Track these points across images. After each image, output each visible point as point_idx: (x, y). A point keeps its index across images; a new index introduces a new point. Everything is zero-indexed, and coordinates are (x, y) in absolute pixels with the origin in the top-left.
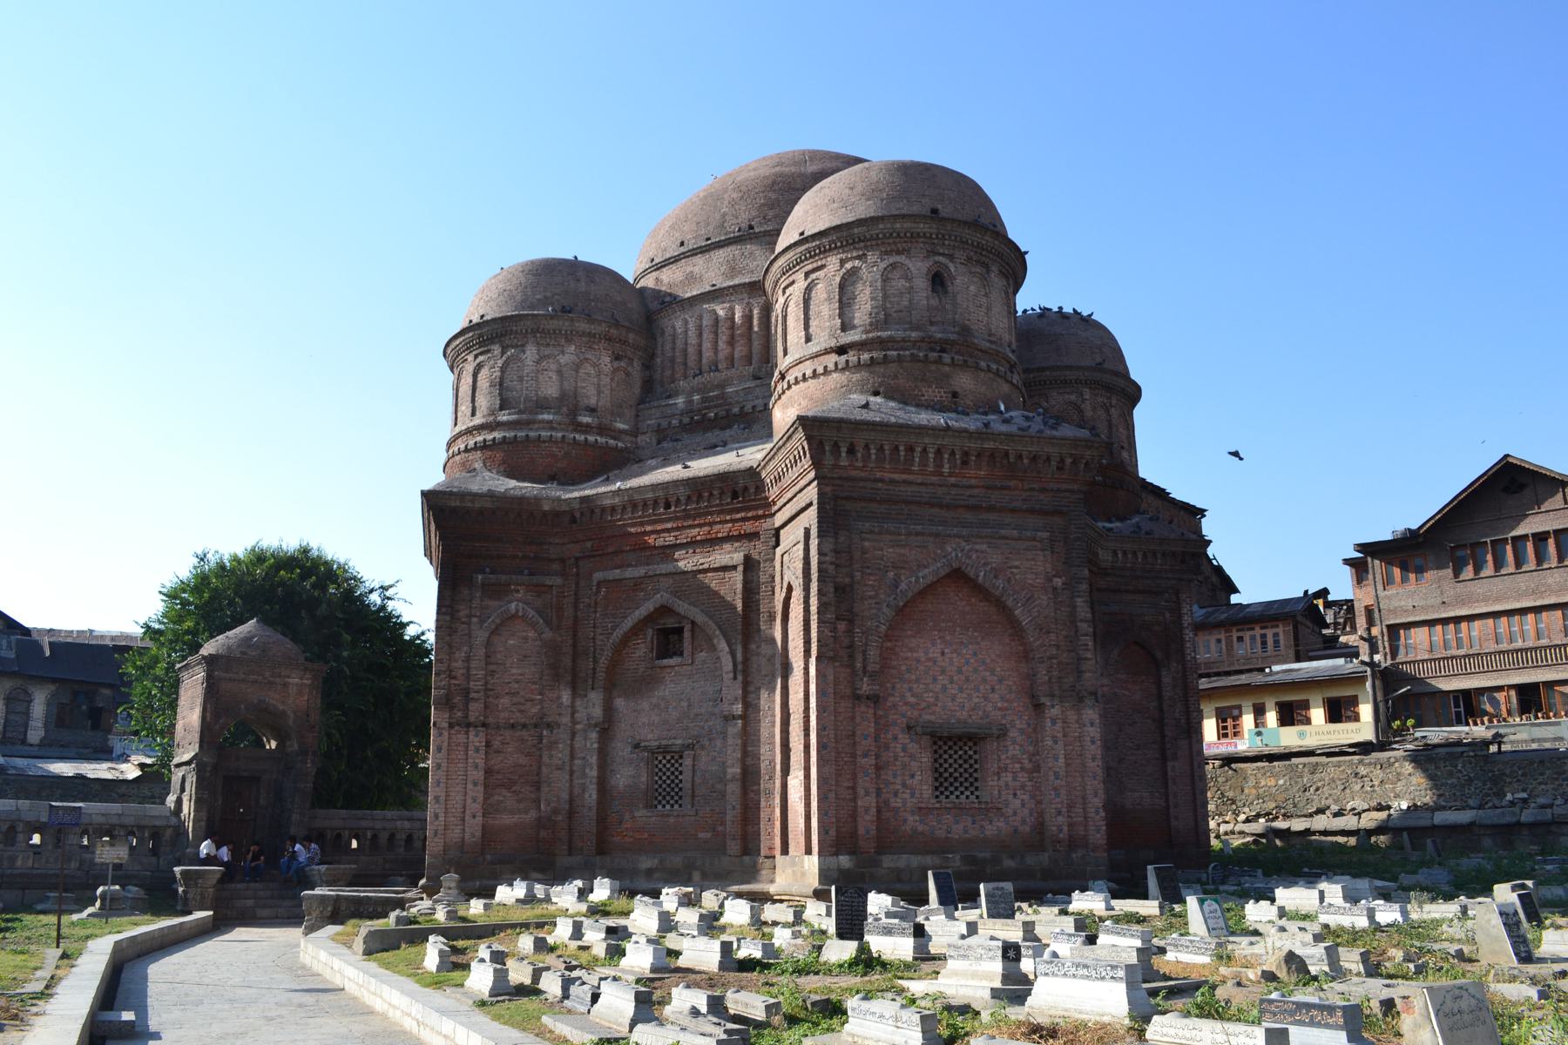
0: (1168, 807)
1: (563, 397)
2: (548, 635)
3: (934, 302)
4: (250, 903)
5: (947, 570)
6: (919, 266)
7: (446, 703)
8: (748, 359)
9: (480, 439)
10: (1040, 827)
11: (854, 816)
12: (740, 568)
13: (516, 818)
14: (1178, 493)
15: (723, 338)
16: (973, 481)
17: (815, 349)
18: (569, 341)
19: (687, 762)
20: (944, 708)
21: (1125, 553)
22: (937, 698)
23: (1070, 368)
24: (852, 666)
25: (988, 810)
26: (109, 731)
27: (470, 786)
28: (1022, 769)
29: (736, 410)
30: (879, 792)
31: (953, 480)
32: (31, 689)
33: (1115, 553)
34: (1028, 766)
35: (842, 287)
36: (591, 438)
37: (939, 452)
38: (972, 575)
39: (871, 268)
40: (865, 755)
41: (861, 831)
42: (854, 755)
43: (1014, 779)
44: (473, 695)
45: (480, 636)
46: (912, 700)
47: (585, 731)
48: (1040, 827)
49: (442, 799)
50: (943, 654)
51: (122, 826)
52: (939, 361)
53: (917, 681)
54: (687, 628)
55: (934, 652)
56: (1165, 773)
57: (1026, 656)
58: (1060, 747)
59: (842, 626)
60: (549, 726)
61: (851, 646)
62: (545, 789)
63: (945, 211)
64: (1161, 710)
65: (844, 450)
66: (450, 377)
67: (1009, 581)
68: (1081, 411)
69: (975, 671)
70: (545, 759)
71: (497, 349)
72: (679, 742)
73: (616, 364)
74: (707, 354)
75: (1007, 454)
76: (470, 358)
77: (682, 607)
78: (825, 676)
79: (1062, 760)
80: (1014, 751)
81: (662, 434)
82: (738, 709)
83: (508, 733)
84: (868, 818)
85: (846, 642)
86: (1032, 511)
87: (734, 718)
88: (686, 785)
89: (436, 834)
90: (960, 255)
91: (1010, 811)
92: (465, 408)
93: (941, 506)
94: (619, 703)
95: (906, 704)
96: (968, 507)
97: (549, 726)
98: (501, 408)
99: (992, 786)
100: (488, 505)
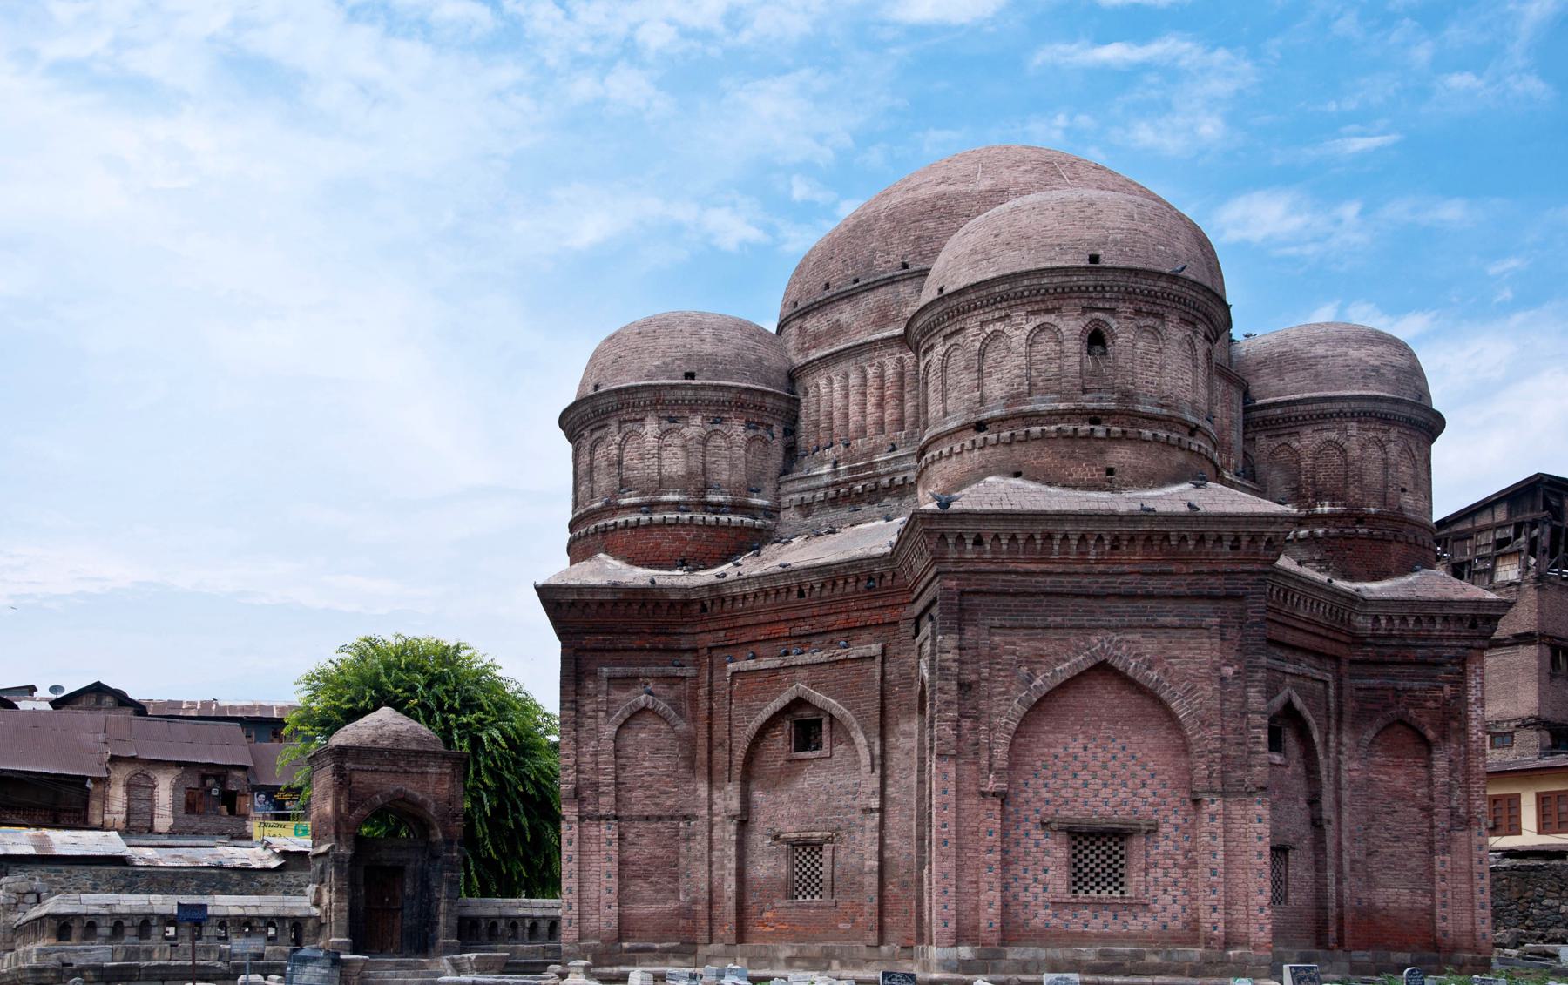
0: (1433, 907)
1: (690, 474)
2: (682, 726)
3: (1089, 365)
5: (1090, 663)
6: (1071, 325)
7: (577, 796)
8: (900, 423)
10: (1193, 925)
12: (879, 659)
13: (654, 908)
15: (872, 400)
16: (1126, 568)
18: (694, 411)
19: (827, 854)
20: (1086, 804)
21: (1390, 619)
22: (1077, 795)
25: (1133, 905)
26: (246, 817)
28: (1175, 865)
29: (885, 481)
30: (1005, 887)
31: (1101, 568)
32: (153, 774)
33: (1376, 619)
34: (1181, 860)
36: (723, 519)
37: (1083, 539)
38: (1120, 666)
41: (984, 924)
45: (609, 730)
49: (575, 890)
50: (1085, 749)
51: (261, 917)
53: (1054, 776)
54: (825, 721)
55: (1076, 747)
56: (1431, 868)
59: (966, 723)
60: (685, 818)
62: (683, 880)
65: (969, 542)
67: (1166, 671)
69: (1124, 766)
70: (683, 850)
73: (751, 433)
74: (854, 418)
75: (1166, 537)
77: (819, 697)
80: (1166, 846)
81: (805, 508)
82: (875, 803)
83: (642, 825)
86: (1200, 597)
87: (872, 811)
88: (826, 877)
93: (1088, 596)
94: (758, 795)
97: (685, 818)
99: (1135, 882)
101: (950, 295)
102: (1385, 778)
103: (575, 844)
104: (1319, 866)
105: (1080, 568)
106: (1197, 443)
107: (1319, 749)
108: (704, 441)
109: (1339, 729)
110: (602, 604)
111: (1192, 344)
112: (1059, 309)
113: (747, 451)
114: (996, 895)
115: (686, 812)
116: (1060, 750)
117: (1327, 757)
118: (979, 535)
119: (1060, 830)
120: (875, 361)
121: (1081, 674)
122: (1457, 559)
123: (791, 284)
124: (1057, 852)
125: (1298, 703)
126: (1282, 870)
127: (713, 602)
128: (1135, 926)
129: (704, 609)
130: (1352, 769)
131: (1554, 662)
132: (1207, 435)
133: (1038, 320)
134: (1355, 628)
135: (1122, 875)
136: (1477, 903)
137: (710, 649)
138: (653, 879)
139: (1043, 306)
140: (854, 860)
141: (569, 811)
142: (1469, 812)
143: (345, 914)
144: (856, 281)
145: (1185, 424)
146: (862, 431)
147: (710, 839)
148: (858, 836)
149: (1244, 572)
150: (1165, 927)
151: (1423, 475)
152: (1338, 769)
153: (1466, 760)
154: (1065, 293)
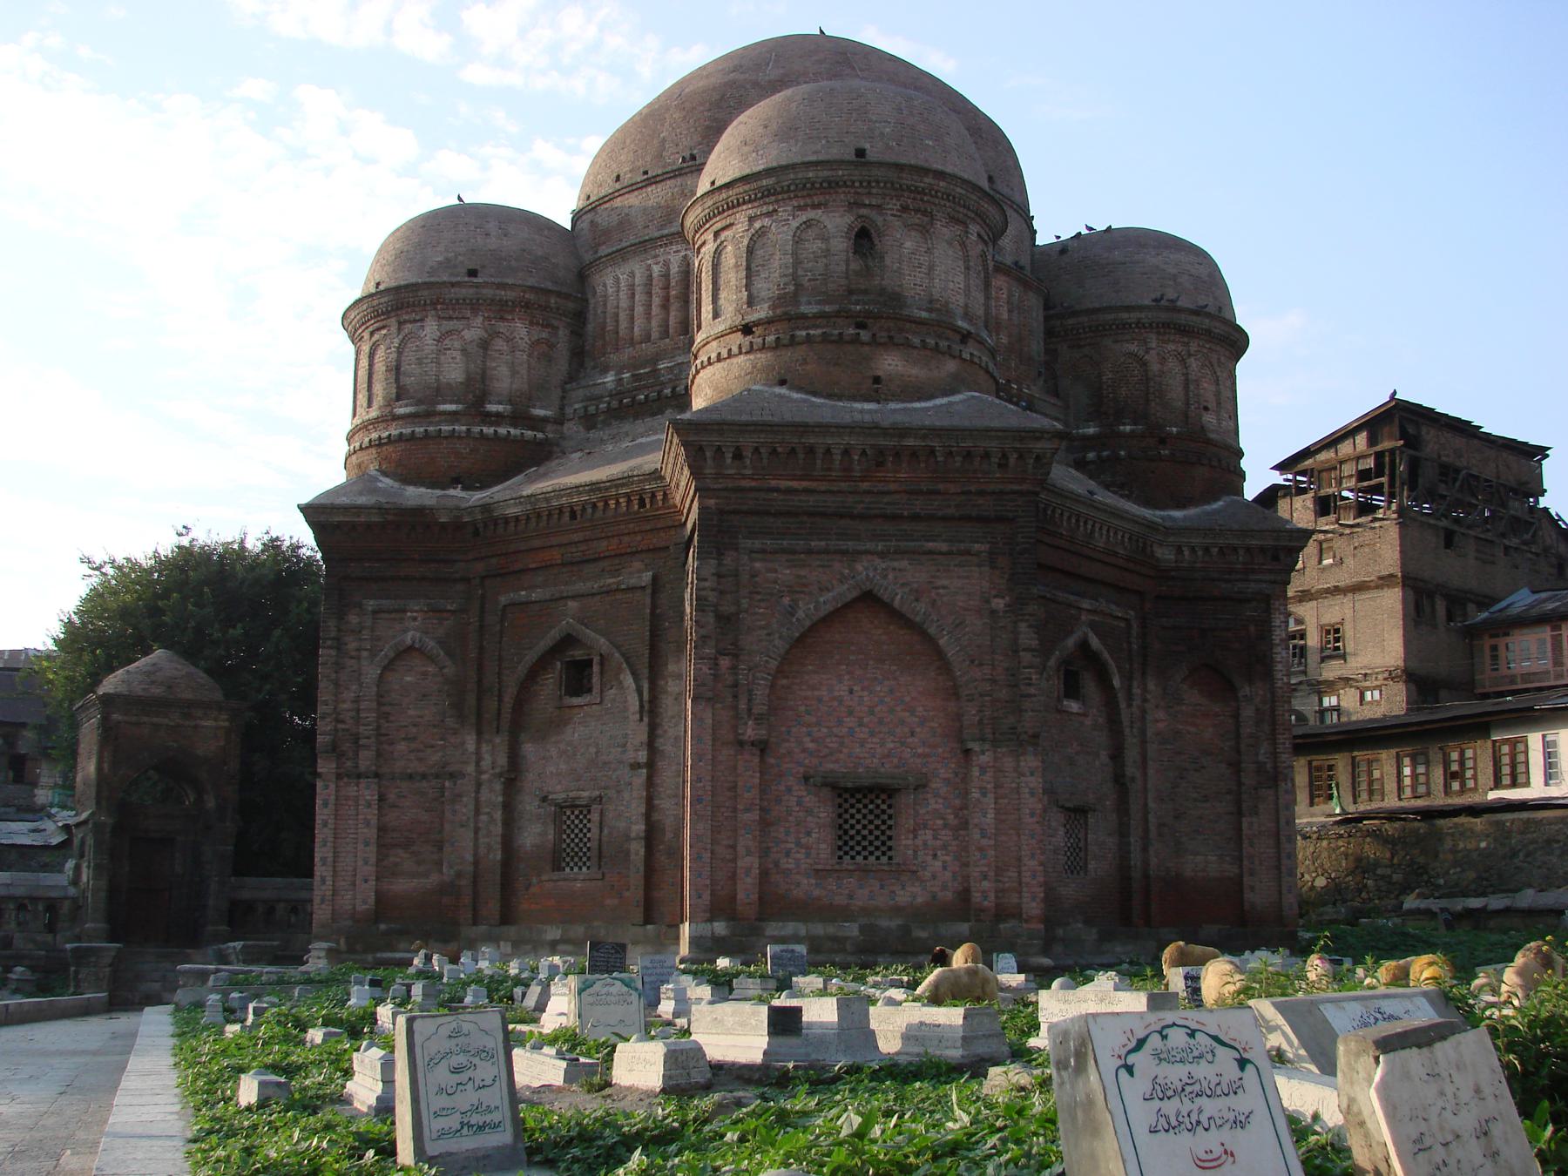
0: (1241, 876)
4: (157, 986)
5: (854, 594)
6: (836, 222)
9: (374, 435)
10: (965, 894)
11: (733, 877)
12: (649, 591)
14: (1493, 425)
16: (892, 487)
17: (721, 328)
19: (595, 817)
21: (1193, 550)
23: (1129, 309)
24: (735, 708)
26: (35, 784)
27: (360, 847)
28: (945, 826)
30: (764, 853)
33: (1179, 550)
35: (750, 251)
36: (502, 431)
38: (886, 598)
39: (783, 227)
40: (747, 810)
42: (735, 810)
43: (935, 838)
44: (363, 741)
45: (371, 672)
46: (811, 745)
47: (490, 781)
48: (965, 894)
50: (851, 692)
52: (856, 340)
54: (596, 660)
55: (841, 690)
56: (1240, 829)
57: (954, 693)
58: (990, 799)
59: (725, 662)
60: (452, 776)
61: (735, 685)
62: (447, 848)
63: (872, 155)
64: (1239, 752)
66: (351, 349)
67: (933, 603)
68: (1145, 364)
70: (448, 815)
71: (393, 321)
72: (585, 794)
76: (366, 335)
78: (701, 720)
79: (991, 816)
80: (934, 804)
81: (589, 421)
82: (643, 756)
84: (749, 880)
85: (729, 680)
86: (969, 518)
89: (323, 901)
90: (893, 205)
91: (928, 874)
92: (362, 398)
93: (852, 517)
94: (529, 749)
95: (804, 750)
96: (885, 517)
97: (452, 776)
98: (398, 398)
99: (904, 843)
100: (375, 519)
101: (721, 188)
102: (1193, 729)
103: (331, 806)
104: (1123, 832)
105: (844, 485)
106: (969, 350)
107: (1121, 696)
108: (485, 345)
109: (1144, 674)
110: (369, 526)
111: (963, 245)
112: (825, 205)
113: (529, 356)
114: (755, 862)
115: (451, 769)
116: (824, 693)
117: (1129, 706)
118: (738, 448)
119: (825, 785)
120: (661, 259)
121: (846, 606)
122: (1322, 493)
123: (593, 175)
124: (823, 813)
125: (1095, 643)
126: (1081, 835)
127: (486, 526)
128: (903, 898)
129: (476, 533)
130: (1159, 722)
131: (1418, 608)
132: (981, 342)
133: (803, 217)
134: (1158, 559)
135: (890, 838)
136: (1283, 868)
137: (483, 578)
138: (415, 848)
139: (809, 201)
140: (622, 825)
141: (325, 766)
142: (1275, 767)
143: (103, 894)
144: (646, 173)
145: (957, 330)
146: (647, 338)
147: (477, 800)
148: (626, 795)
149: (1014, 492)
150: (934, 897)
151: (1226, 393)
152: (1143, 719)
153: (1273, 710)
154: (832, 185)
